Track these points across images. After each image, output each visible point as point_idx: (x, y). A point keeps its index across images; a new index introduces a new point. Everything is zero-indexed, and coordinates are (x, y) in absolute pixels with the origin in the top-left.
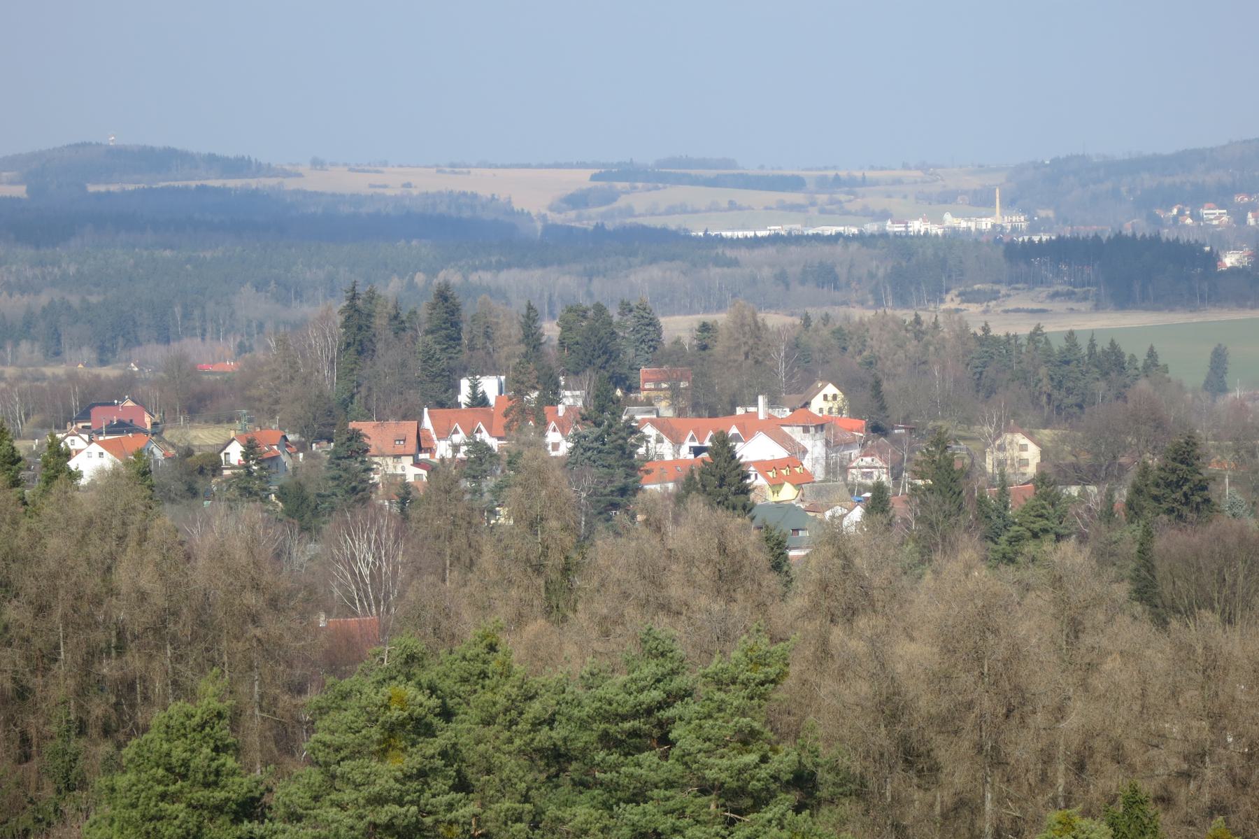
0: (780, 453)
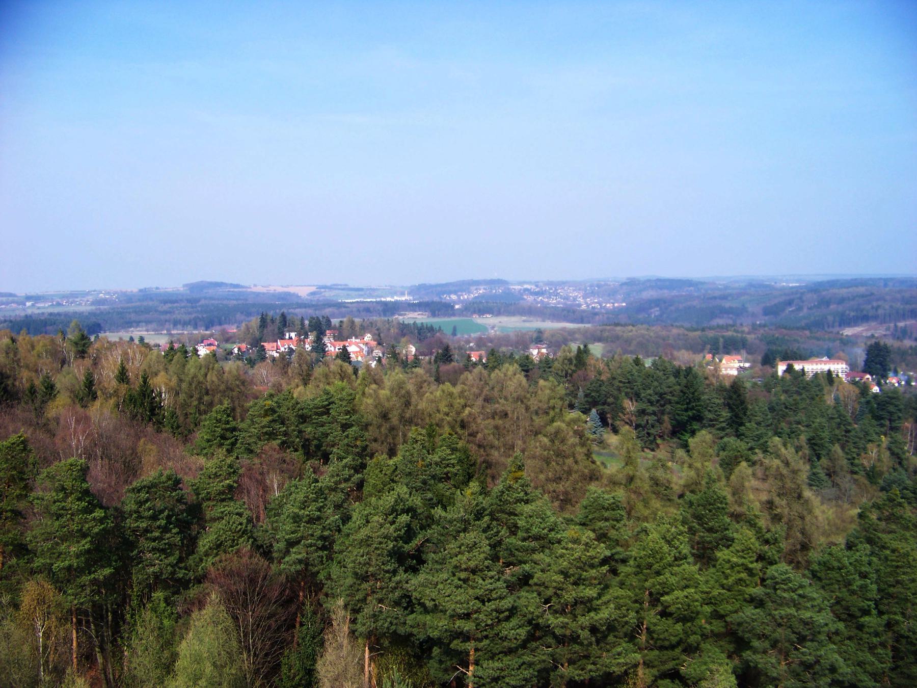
0: (358, 349)
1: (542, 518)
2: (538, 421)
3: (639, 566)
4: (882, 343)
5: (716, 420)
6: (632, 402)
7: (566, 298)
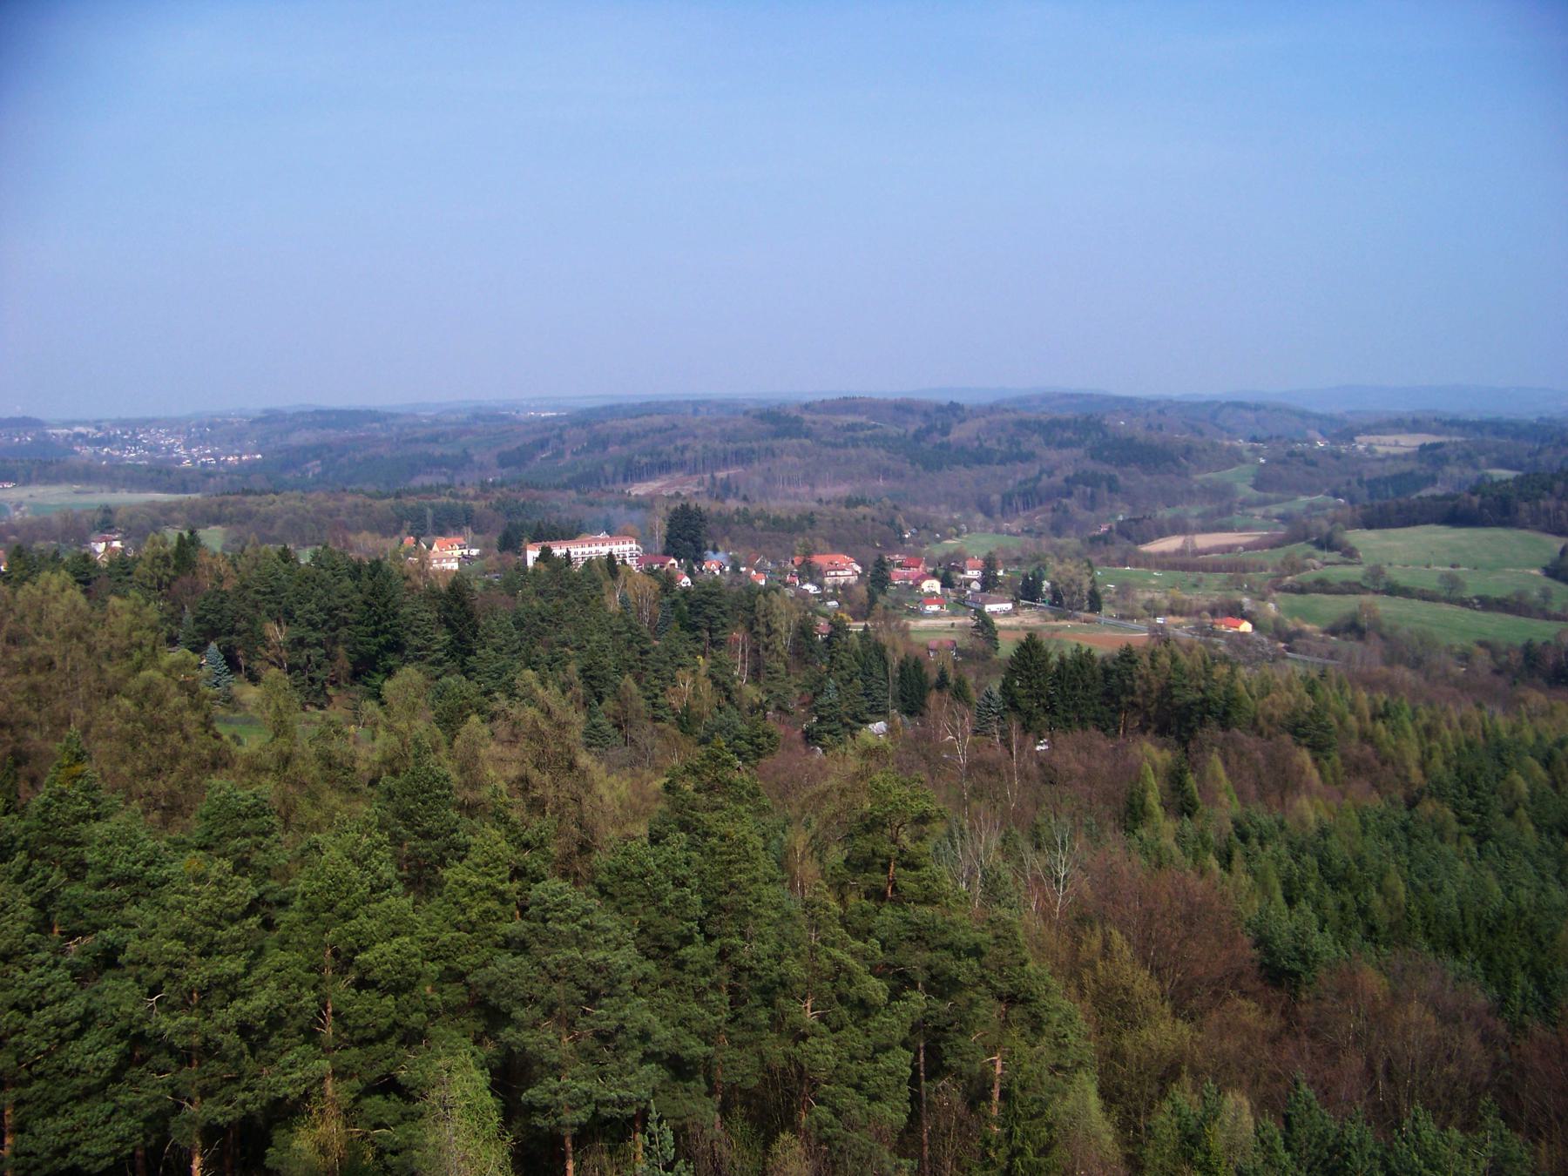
1: (130, 844)
2: (113, 671)
3: (311, 908)
4: (692, 506)
5: (426, 648)
6: (279, 625)
7: (155, 448)
